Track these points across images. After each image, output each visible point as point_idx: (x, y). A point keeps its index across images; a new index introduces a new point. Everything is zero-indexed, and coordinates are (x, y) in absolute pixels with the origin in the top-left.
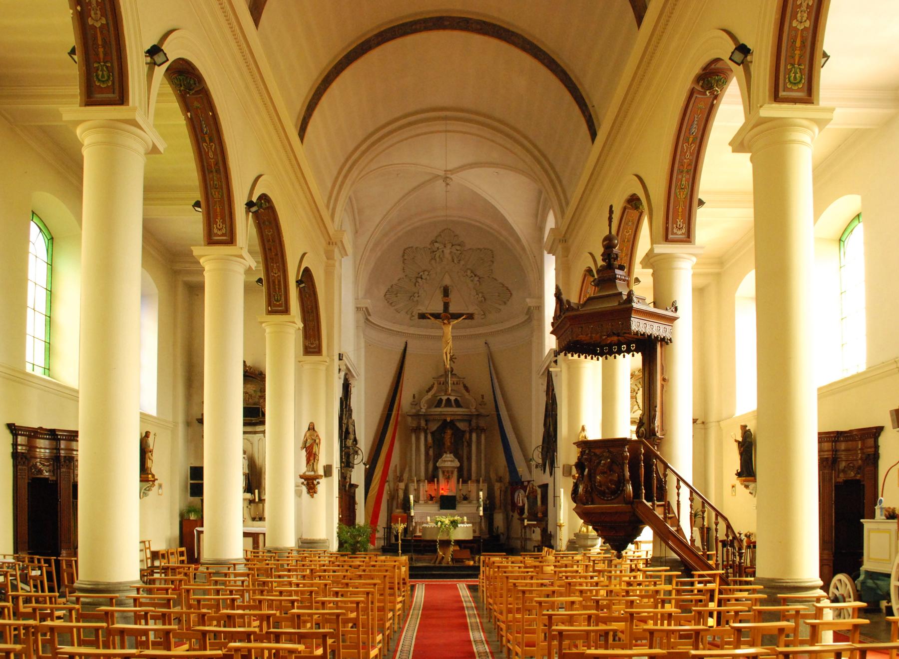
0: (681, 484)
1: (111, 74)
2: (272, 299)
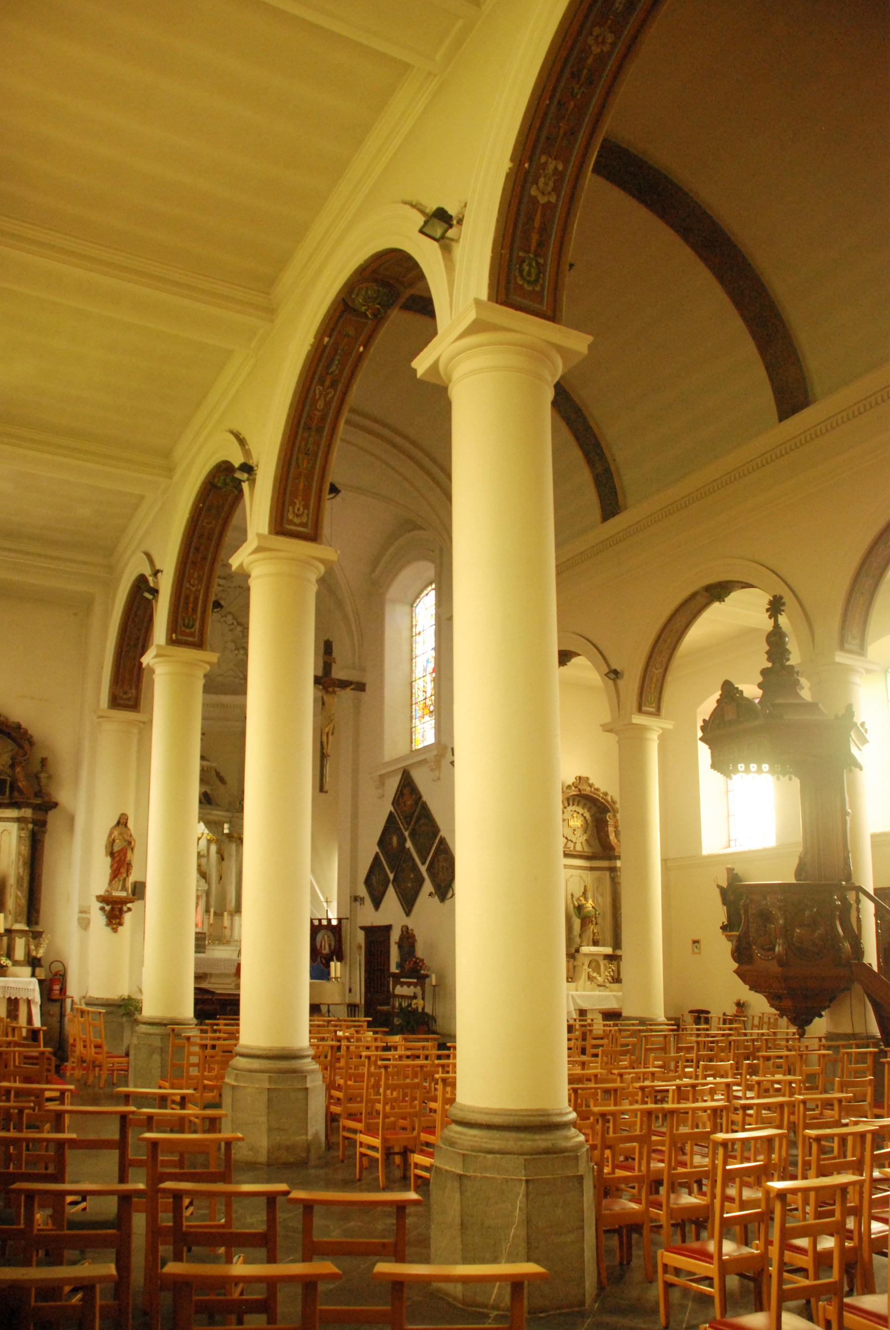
1: (542, 275)
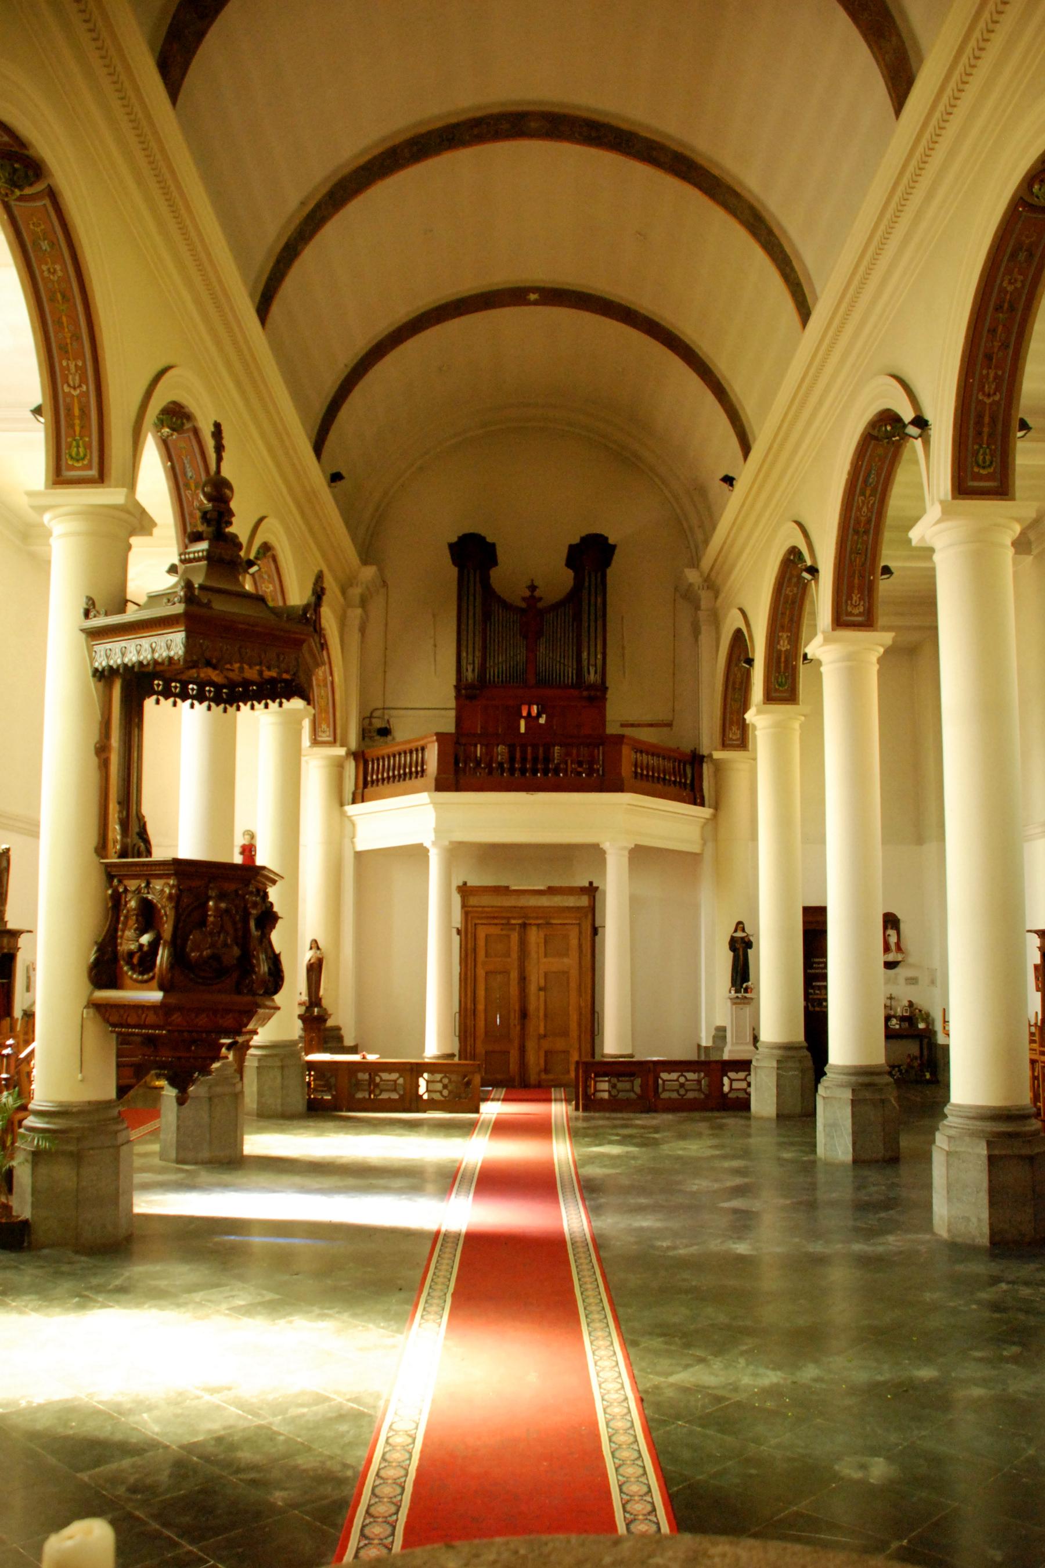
2: (65, 456)
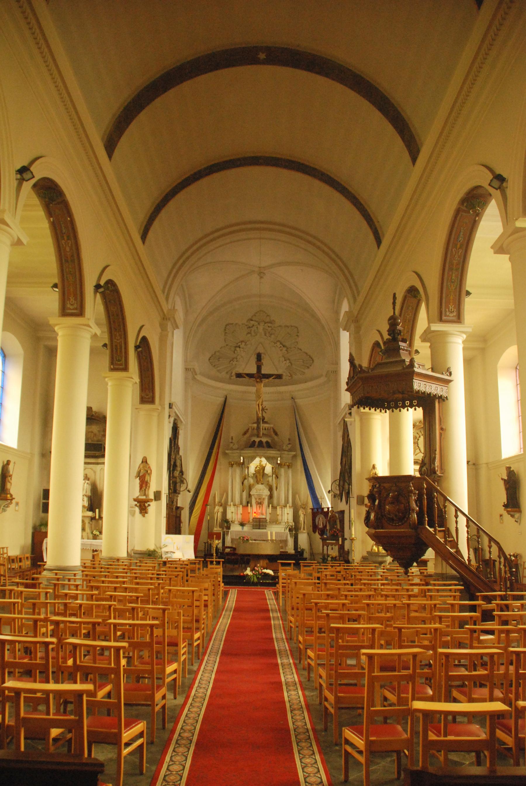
0: (459, 513)
